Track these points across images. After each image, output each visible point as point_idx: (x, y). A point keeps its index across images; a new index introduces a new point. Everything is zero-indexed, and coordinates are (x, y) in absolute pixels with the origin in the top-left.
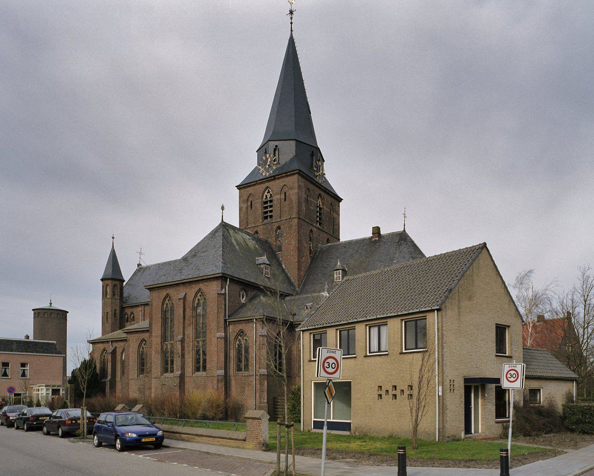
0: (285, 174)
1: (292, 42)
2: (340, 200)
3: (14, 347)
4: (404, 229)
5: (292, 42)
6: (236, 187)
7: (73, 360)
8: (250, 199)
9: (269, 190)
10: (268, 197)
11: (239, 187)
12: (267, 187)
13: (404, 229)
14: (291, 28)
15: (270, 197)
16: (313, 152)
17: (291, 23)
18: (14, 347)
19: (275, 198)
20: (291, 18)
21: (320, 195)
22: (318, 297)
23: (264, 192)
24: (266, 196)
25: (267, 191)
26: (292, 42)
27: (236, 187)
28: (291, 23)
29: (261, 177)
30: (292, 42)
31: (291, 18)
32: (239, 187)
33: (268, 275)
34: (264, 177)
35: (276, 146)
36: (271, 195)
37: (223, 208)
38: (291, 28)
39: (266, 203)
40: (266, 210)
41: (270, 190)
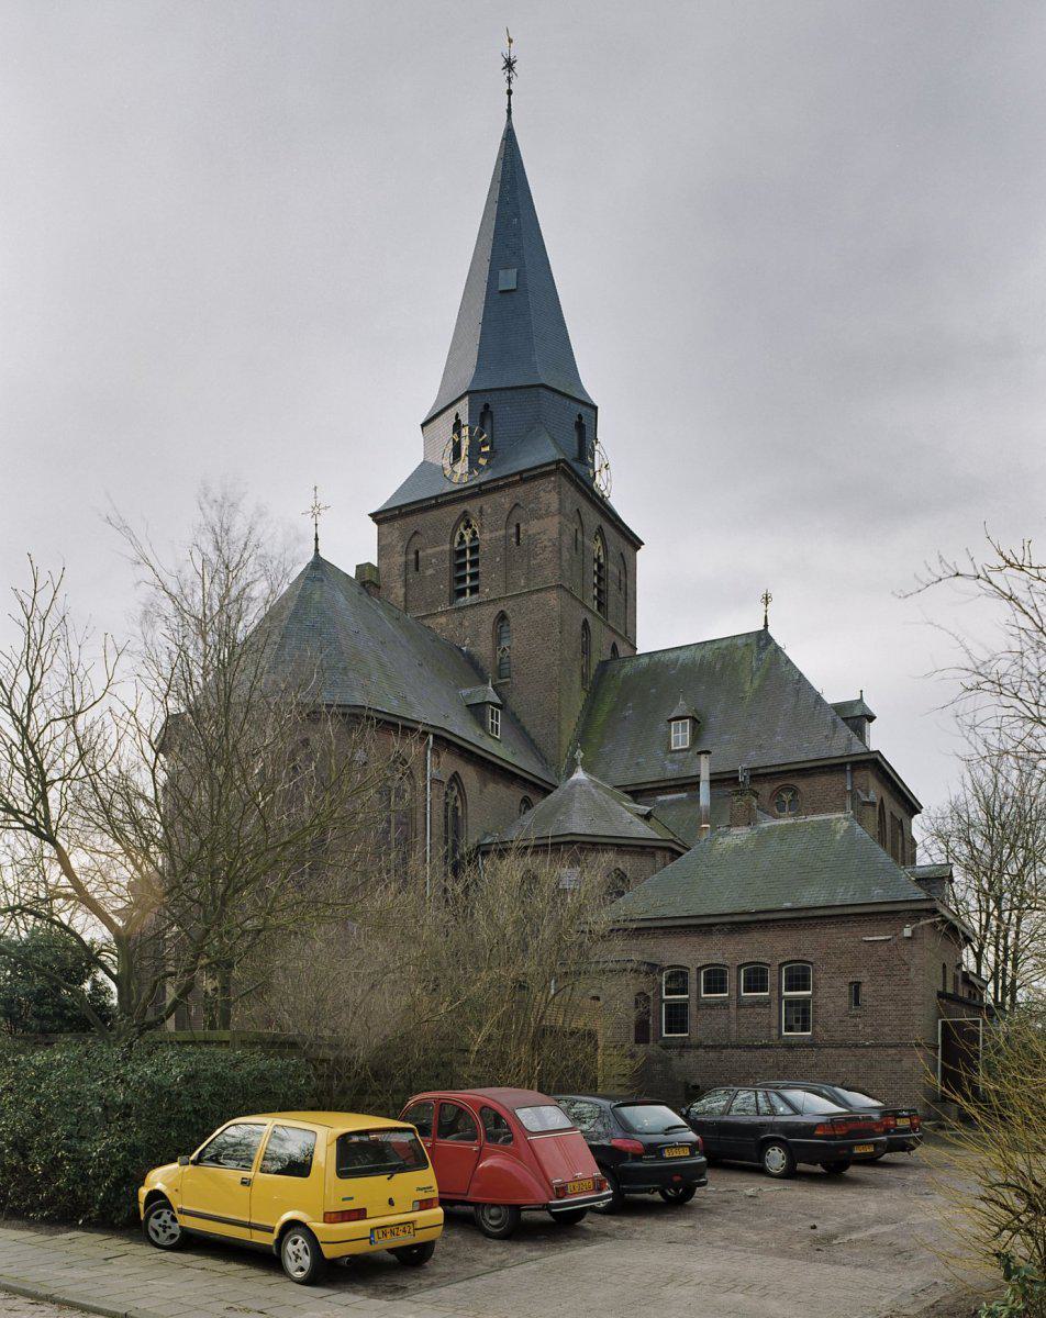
0: (518, 478)
1: (509, 138)
2: (636, 543)
3: (776, 1158)
4: (766, 626)
5: (509, 138)
6: (370, 515)
7: (158, 1294)
8: (413, 549)
9: (468, 521)
10: (467, 538)
11: (377, 517)
13: (766, 626)
14: (509, 105)
15: (471, 540)
16: (580, 416)
17: (510, 92)
18: (776, 1158)
19: (485, 537)
20: (509, 80)
21: (600, 531)
22: (681, 665)
23: (456, 526)
24: (462, 536)
26: (509, 138)
27: (370, 515)
28: (510, 92)
29: (449, 488)
30: (509, 138)
31: (509, 80)
32: (377, 517)
33: (493, 710)
34: (458, 487)
35: (487, 406)
36: (474, 533)
37: (509, 65)
38: (509, 105)
39: (462, 553)
40: (461, 587)
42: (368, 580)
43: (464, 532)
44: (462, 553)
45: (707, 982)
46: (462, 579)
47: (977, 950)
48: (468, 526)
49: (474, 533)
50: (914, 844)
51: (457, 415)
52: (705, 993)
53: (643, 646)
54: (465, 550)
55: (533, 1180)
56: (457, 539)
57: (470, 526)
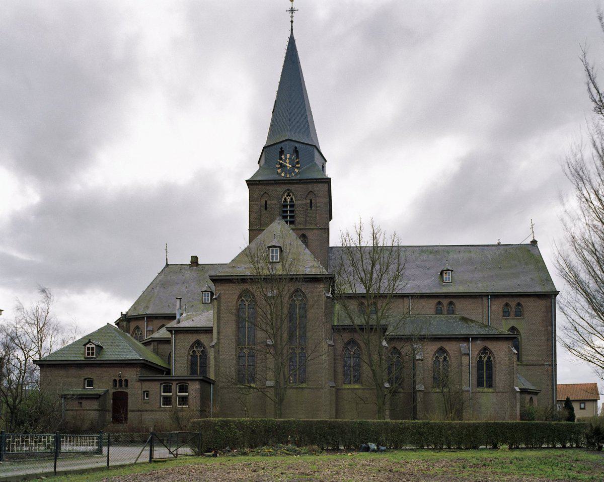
1: (292, 42)
5: (292, 42)
12: (288, 190)
14: (292, 26)
15: (290, 202)
24: (285, 199)
25: (286, 194)
26: (292, 41)
30: (292, 41)
32: (249, 183)
36: (292, 199)
38: (292, 26)
41: (291, 194)
42: (504, 442)
43: (287, 198)
44: (286, 206)
45: (180, 389)
46: (286, 212)
47: (368, 363)
48: (289, 195)
49: (292, 199)
50: (73, 343)
51: (282, 148)
52: (180, 404)
53: (330, 246)
54: (287, 205)
55: (525, 422)
56: (283, 199)
57: (290, 196)
